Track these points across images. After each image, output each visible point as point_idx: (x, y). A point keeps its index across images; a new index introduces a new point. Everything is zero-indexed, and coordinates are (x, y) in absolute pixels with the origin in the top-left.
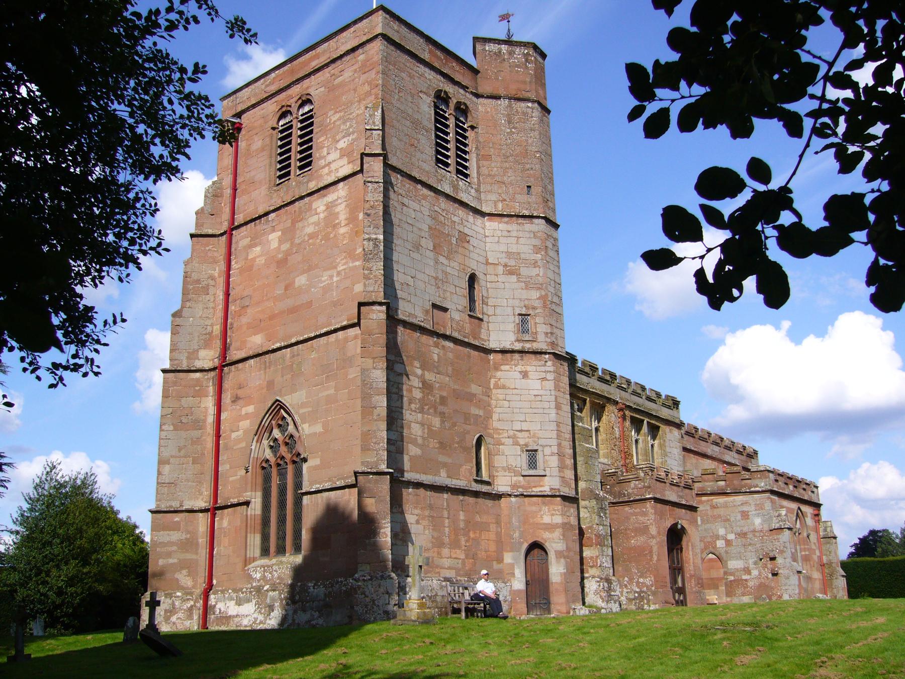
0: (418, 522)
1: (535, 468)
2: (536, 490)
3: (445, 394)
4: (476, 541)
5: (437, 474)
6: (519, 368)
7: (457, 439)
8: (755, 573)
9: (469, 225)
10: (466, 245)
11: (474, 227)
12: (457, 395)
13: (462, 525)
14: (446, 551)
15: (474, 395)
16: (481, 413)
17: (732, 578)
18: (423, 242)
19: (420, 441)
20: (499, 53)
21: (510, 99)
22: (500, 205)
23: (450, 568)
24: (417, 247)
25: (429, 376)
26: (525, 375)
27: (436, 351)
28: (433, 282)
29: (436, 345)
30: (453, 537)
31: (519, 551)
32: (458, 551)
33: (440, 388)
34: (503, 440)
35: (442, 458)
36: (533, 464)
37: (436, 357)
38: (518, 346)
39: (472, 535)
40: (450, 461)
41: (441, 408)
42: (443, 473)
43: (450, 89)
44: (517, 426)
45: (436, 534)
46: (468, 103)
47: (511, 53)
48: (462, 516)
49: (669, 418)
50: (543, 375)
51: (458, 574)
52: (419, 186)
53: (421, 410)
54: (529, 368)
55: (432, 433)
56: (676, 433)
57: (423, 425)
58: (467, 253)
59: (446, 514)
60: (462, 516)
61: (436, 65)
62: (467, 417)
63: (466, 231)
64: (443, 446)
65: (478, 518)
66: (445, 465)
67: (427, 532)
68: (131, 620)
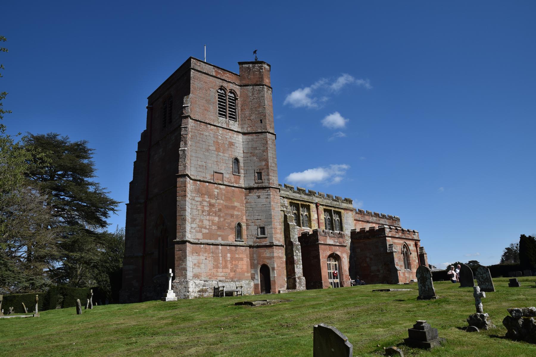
0: (206, 259)
1: (264, 234)
2: (264, 243)
3: (221, 207)
4: (236, 266)
5: (217, 239)
6: (257, 194)
7: (227, 225)
8: (382, 271)
9: (234, 138)
10: (233, 147)
11: (237, 139)
12: (227, 207)
13: (229, 259)
14: (220, 270)
15: (236, 207)
16: (240, 213)
17: (373, 274)
18: (211, 148)
19: (208, 227)
20: (249, 68)
21: (253, 85)
22: (249, 129)
23: (223, 276)
24: (208, 150)
25: (213, 201)
26: (259, 197)
27: (216, 190)
28: (215, 163)
29: (217, 188)
30: (224, 263)
31: (257, 268)
32: (227, 270)
33: (218, 206)
34: (250, 224)
35: (219, 233)
36: (263, 232)
37: (216, 193)
38: (256, 186)
39: (234, 262)
40: (223, 234)
41: (219, 213)
42: (220, 239)
43: (225, 84)
44: (256, 217)
45: (215, 263)
46: (235, 89)
47: (254, 67)
48: (229, 255)
49: (346, 208)
50: (267, 196)
51: (226, 279)
52: (209, 126)
53: (209, 215)
54: (260, 194)
55: (213, 223)
56: (350, 213)
57: (209, 220)
58: (233, 150)
59: (220, 255)
60: (229, 255)
61: (219, 76)
62: (232, 216)
63: (233, 141)
64: (219, 228)
65: (237, 256)
66: (220, 236)
67: (211, 263)
68: (531, 324)
